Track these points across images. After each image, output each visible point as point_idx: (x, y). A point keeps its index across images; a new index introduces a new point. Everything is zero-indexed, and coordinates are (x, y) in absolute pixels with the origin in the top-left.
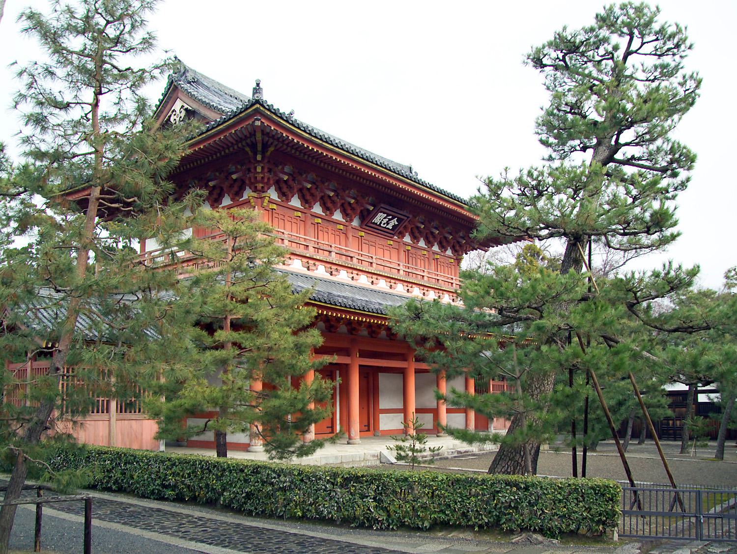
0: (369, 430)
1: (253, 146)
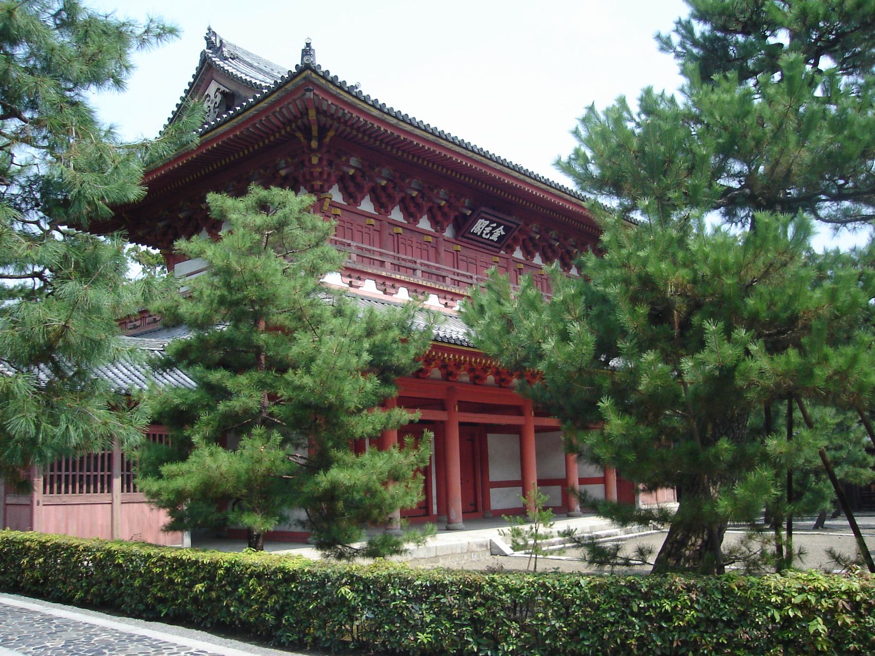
0: (476, 510)
1: (307, 131)
